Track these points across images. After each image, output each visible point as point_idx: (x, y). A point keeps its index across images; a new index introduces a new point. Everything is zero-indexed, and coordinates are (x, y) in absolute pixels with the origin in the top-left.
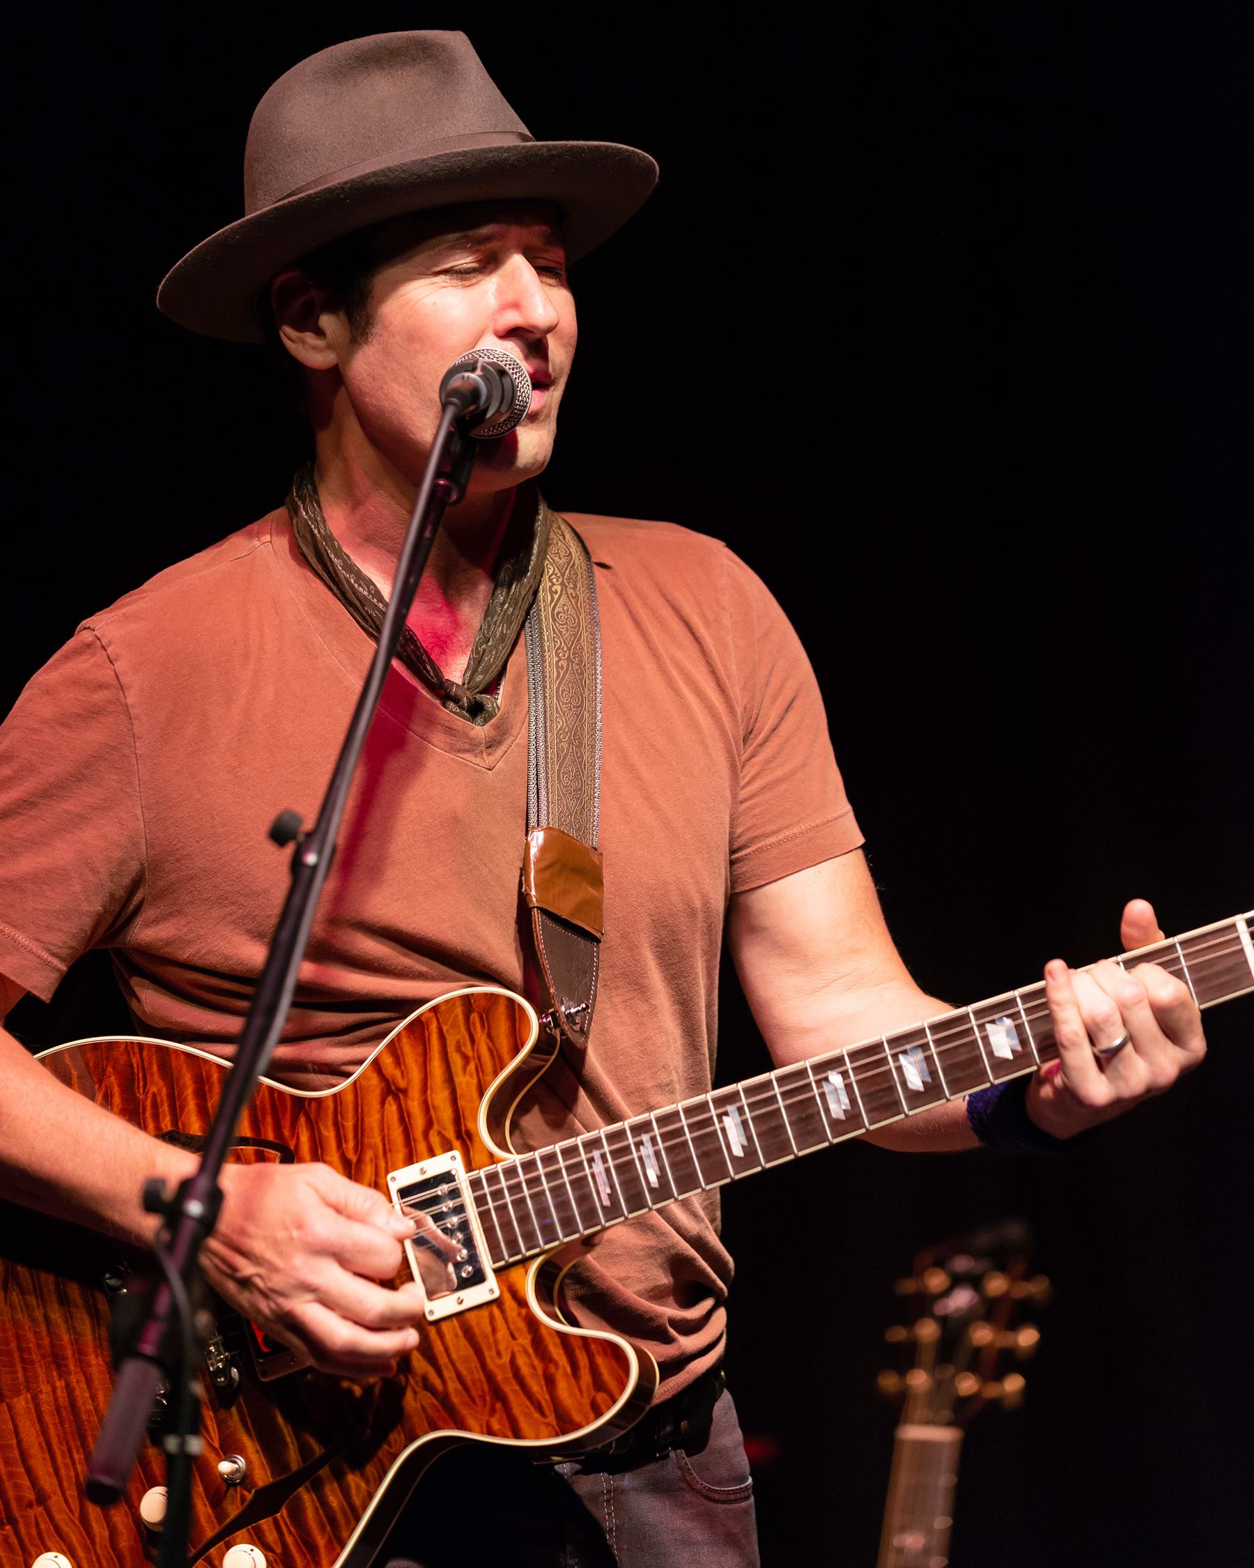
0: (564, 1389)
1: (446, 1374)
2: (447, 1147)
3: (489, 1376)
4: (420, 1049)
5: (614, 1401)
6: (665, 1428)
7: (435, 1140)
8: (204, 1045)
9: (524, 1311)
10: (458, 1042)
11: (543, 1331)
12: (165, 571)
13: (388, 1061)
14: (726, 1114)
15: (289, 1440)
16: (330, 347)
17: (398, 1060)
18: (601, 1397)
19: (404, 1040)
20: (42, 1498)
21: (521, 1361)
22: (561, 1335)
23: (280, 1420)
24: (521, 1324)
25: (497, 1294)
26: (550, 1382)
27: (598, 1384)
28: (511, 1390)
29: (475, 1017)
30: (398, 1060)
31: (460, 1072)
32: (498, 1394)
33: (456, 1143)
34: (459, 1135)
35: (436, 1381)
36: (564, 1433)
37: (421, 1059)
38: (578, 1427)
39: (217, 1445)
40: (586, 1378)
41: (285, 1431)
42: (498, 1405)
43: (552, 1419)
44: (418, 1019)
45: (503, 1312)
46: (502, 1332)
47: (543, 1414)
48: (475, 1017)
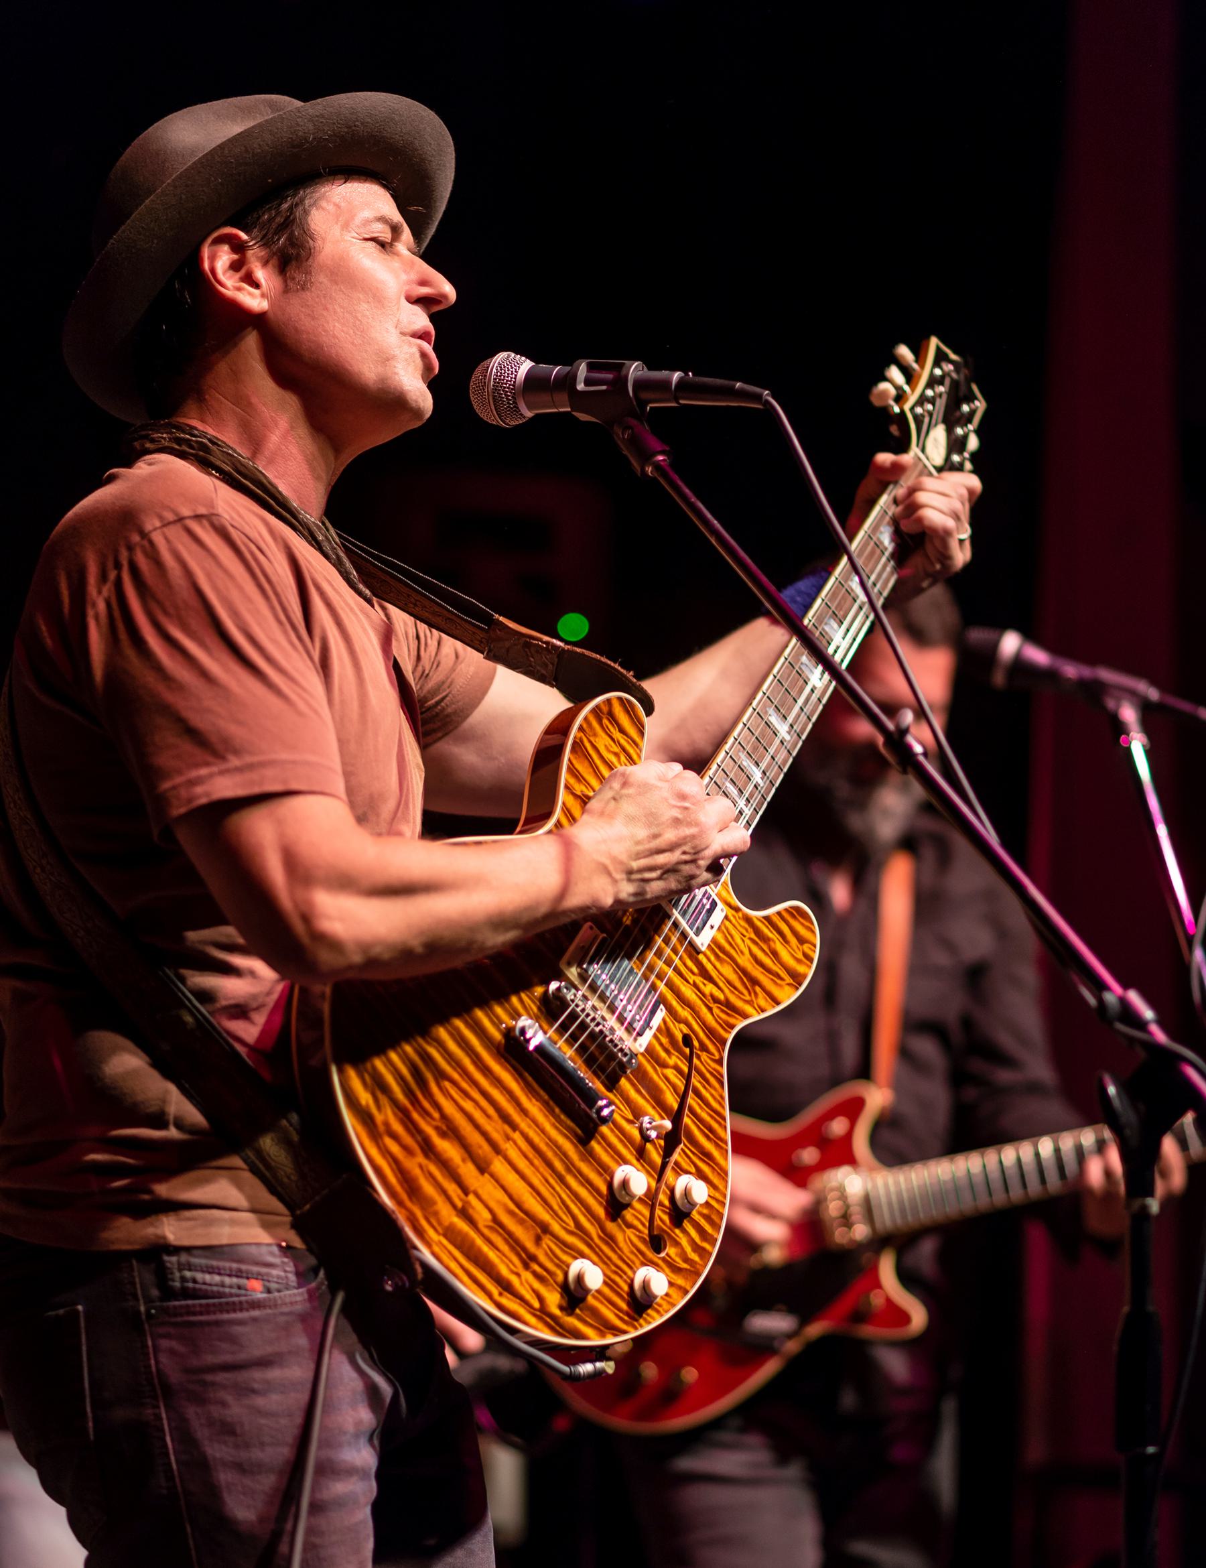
1: (721, 984)
4: (586, 763)
6: (1019, 665)
15: (664, 1087)
16: (263, 296)
18: (806, 947)
19: (574, 762)
20: (545, 1229)
21: (755, 949)
23: (49, 641)
24: (743, 923)
26: (775, 954)
27: (802, 941)
28: (757, 973)
29: (605, 722)
32: (755, 982)
35: (722, 997)
39: (631, 1117)
41: (46, 634)
42: (758, 989)
43: (789, 980)
44: (575, 742)
47: (782, 979)
48: (605, 722)
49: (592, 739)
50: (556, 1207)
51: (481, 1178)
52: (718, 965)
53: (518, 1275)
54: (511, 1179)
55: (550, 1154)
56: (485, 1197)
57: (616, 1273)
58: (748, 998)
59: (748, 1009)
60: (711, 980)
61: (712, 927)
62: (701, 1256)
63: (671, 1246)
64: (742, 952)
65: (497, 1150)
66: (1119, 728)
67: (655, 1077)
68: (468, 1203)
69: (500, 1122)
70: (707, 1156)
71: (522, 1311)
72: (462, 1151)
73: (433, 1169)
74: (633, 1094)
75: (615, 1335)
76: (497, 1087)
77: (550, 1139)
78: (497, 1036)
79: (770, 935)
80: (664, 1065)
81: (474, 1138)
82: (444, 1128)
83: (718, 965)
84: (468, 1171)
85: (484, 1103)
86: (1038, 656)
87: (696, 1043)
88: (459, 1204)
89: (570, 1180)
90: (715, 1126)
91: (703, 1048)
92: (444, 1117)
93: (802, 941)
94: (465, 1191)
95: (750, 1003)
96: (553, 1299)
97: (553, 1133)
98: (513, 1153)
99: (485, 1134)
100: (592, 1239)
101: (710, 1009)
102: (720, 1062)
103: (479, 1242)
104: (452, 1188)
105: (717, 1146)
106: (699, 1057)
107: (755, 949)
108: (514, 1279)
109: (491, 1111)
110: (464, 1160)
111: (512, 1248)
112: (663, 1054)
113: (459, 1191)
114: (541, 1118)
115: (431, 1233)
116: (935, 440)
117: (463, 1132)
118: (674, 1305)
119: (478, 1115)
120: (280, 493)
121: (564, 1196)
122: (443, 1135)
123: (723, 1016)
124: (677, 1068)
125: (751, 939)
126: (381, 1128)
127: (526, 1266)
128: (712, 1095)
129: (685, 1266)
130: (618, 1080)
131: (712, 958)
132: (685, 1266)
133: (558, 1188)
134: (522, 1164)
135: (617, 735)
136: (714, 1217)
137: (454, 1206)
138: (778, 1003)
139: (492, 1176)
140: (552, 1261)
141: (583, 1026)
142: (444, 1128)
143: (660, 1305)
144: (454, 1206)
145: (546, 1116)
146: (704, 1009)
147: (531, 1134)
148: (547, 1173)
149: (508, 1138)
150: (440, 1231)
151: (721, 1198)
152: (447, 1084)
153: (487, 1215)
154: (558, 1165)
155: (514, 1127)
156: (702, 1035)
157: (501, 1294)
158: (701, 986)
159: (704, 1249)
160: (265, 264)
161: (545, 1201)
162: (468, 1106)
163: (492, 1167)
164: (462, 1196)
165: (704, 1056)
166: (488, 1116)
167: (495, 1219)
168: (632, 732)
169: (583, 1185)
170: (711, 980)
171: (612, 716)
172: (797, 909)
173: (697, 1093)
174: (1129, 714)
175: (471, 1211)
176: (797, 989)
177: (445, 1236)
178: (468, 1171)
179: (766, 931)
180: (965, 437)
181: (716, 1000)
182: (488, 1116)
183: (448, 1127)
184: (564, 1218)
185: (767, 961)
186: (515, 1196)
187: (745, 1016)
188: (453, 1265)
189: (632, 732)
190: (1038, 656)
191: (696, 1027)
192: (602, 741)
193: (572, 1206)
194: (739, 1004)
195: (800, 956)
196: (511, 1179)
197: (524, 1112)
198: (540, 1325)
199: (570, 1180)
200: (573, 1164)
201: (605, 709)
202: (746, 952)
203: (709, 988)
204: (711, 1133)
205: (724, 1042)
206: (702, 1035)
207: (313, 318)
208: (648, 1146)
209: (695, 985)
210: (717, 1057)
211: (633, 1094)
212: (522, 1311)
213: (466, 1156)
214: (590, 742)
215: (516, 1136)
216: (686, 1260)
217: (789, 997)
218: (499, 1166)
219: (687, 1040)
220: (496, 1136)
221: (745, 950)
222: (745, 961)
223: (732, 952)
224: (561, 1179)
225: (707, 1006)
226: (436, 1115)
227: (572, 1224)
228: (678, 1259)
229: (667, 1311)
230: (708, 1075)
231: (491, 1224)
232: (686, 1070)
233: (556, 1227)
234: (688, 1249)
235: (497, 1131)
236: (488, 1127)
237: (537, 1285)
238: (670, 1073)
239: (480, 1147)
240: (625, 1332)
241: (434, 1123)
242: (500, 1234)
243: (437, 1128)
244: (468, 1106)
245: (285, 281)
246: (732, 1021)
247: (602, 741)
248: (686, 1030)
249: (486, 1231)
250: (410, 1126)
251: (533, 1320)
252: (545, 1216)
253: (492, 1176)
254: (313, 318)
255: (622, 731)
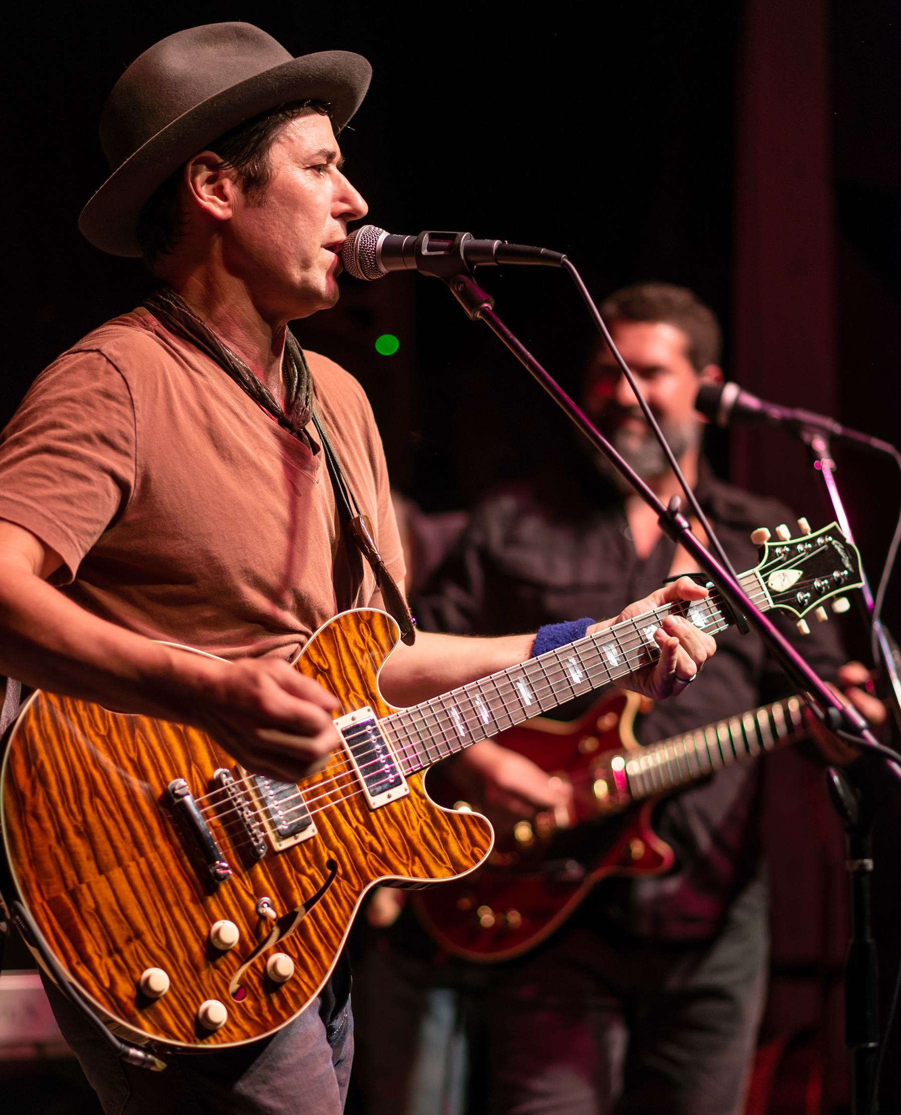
0: (454, 846)
1: (383, 841)
2: (363, 705)
3: (409, 842)
4: (332, 646)
5: (485, 852)
6: (737, 409)
7: (355, 703)
8: (204, 648)
9: (424, 801)
10: (355, 641)
11: (437, 812)
12: (336, 365)
13: (313, 652)
14: (518, 681)
15: (294, 886)
16: (229, 206)
17: (320, 652)
18: (476, 850)
20: (138, 935)
21: (426, 830)
22: (446, 813)
24: (423, 808)
25: (408, 792)
26: (445, 843)
27: (474, 843)
28: (422, 848)
29: (362, 626)
30: (320, 652)
31: (360, 659)
32: (416, 853)
33: (367, 702)
34: (367, 697)
35: (380, 850)
36: (459, 873)
37: (334, 652)
38: (467, 869)
39: (252, 892)
40: (467, 841)
42: (417, 859)
43: (449, 865)
45: (412, 802)
46: (414, 816)
48: (362, 626)
49: (345, 632)
50: (154, 924)
51: (98, 876)
52: (386, 826)
53: (100, 957)
55: (165, 885)
56: (95, 891)
57: (189, 994)
58: (405, 861)
59: (402, 869)
60: (374, 833)
61: (389, 797)
62: (274, 1018)
63: (250, 999)
64: (413, 828)
65: (120, 862)
66: (813, 455)
67: (288, 875)
68: (80, 890)
69: (132, 845)
70: (315, 953)
71: (92, 984)
72: (90, 851)
73: (59, 852)
74: (261, 876)
75: (168, 1037)
76: (140, 820)
77: (170, 874)
78: (159, 792)
79: (446, 827)
80: (302, 871)
81: (104, 846)
82: (82, 829)
83: (386, 826)
84: (89, 867)
85: (123, 826)
86: (751, 402)
87: (340, 870)
88: (71, 886)
89: (176, 911)
90: (332, 935)
91: (346, 876)
92: (85, 821)
94: (81, 880)
95: (406, 866)
96: (125, 989)
97: (175, 872)
98: (133, 870)
100: (177, 961)
101: (365, 854)
102: (358, 894)
103: (77, 919)
104: (70, 873)
105: (327, 949)
106: (338, 882)
107: (426, 830)
108: (96, 960)
109: (127, 834)
110: (88, 858)
111: (103, 936)
112: (303, 863)
113: (75, 878)
114: (169, 857)
115: (37, 895)
117: (97, 839)
118: (232, 1041)
119: (114, 832)
121: (165, 920)
122: (79, 833)
123: (376, 864)
124: (312, 878)
125: (425, 822)
126: (29, 808)
127: (110, 954)
128: (339, 913)
129: (256, 1018)
130: (254, 864)
131: (382, 819)
132: (256, 1018)
133: (162, 912)
134: (138, 882)
135: (369, 638)
136: (300, 997)
137: (66, 886)
138: (431, 876)
139: (108, 879)
140: (134, 960)
141: (229, 805)
142: (82, 829)
143: (220, 1035)
144: (66, 886)
145: (174, 858)
146: (359, 851)
147: (157, 865)
148: (157, 898)
149: (133, 859)
150: (46, 896)
151: (312, 986)
152: (98, 802)
153: (91, 903)
154: (170, 897)
155: (142, 853)
156: (349, 867)
157: (78, 963)
158: (363, 833)
159: (280, 1015)
160: (234, 183)
161: (146, 916)
162: (109, 823)
163: (111, 873)
164: (76, 882)
165: (344, 883)
166: (123, 837)
167: (97, 910)
168: (383, 642)
169: (186, 920)
170: (374, 833)
171: (369, 624)
172: (481, 821)
173: (325, 905)
174: (820, 445)
175: (79, 896)
176: (454, 874)
177: (48, 903)
178: (89, 867)
179: (443, 822)
181: (373, 849)
182: (123, 837)
183: (85, 830)
184: (159, 935)
185: (435, 844)
186: (122, 901)
187: (396, 872)
188: (46, 926)
189: (383, 642)
190: (751, 402)
191: (345, 859)
192: (353, 636)
193: (170, 930)
194: (395, 862)
195: (468, 853)
198: (103, 1000)
199: (176, 911)
200: (183, 901)
201: (366, 617)
202: (418, 828)
203: (369, 838)
204: (325, 937)
205: (368, 881)
206: (349, 867)
207: (264, 230)
208: (263, 924)
209: (356, 830)
210: (357, 888)
211: (261, 876)
212: (92, 984)
213: (92, 856)
214: (342, 633)
215: (142, 861)
216: (259, 1013)
217: (443, 877)
218: (117, 874)
219: (332, 864)
220: (123, 852)
221: (416, 827)
223: (404, 822)
224: (168, 907)
225: (362, 849)
226: (79, 818)
227: (164, 941)
228: (251, 1011)
229: (224, 1042)
230: (342, 898)
231: (92, 912)
232: (322, 884)
233: (149, 938)
234: (265, 1009)
235: (126, 850)
236: (119, 844)
237: (114, 971)
238: (305, 880)
239: (107, 855)
240: (178, 1039)
241: (75, 823)
242: (97, 922)
243: (75, 827)
244: (109, 823)
245: (247, 198)
246: (382, 870)
247: (353, 636)
248: (333, 856)
249: (87, 916)
250: (54, 817)
251: (98, 994)
252: (142, 926)
253: (108, 879)
254: (264, 230)
255: (375, 637)
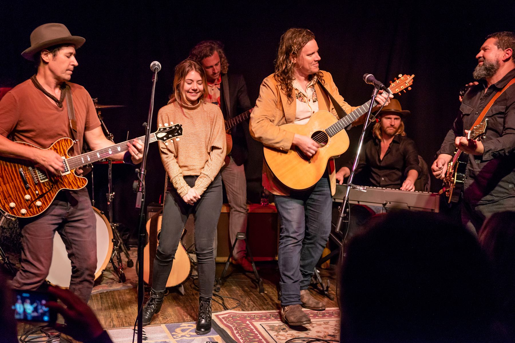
20: (10, 196)
26: (77, 183)
27: (83, 183)
28: (72, 184)
32: (71, 184)
54: (8, 187)
65: (8, 183)
93: (83, 183)
98: (11, 184)
99: (8, 180)
116: (275, 296)
120: (244, 221)
134: (12, 187)
155: (13, 181)
171: (67, 141)
173: (50, 193)
180: (454, 180)
196: (8, 187)
197: (16, 180)
218: (7, 185)
220: (9, 181)
222: (70, 181)
233: (12, 197)
252: (11, 195)
